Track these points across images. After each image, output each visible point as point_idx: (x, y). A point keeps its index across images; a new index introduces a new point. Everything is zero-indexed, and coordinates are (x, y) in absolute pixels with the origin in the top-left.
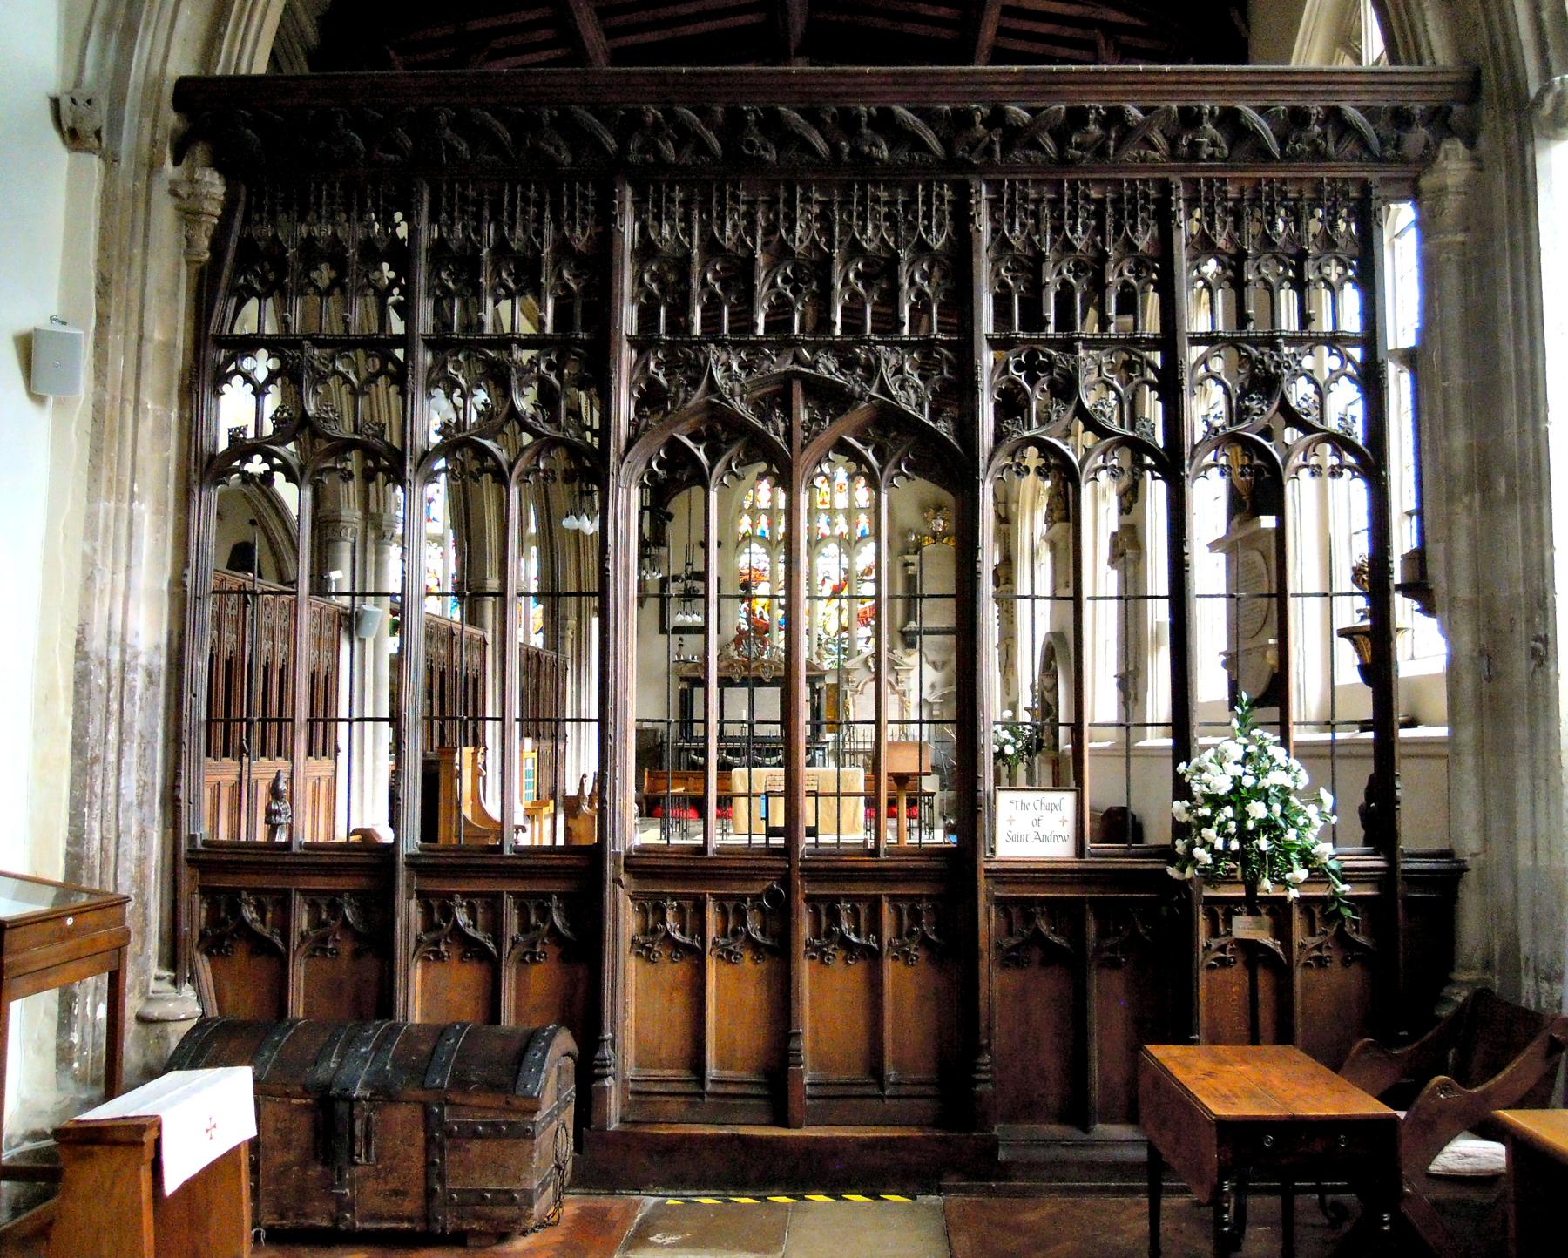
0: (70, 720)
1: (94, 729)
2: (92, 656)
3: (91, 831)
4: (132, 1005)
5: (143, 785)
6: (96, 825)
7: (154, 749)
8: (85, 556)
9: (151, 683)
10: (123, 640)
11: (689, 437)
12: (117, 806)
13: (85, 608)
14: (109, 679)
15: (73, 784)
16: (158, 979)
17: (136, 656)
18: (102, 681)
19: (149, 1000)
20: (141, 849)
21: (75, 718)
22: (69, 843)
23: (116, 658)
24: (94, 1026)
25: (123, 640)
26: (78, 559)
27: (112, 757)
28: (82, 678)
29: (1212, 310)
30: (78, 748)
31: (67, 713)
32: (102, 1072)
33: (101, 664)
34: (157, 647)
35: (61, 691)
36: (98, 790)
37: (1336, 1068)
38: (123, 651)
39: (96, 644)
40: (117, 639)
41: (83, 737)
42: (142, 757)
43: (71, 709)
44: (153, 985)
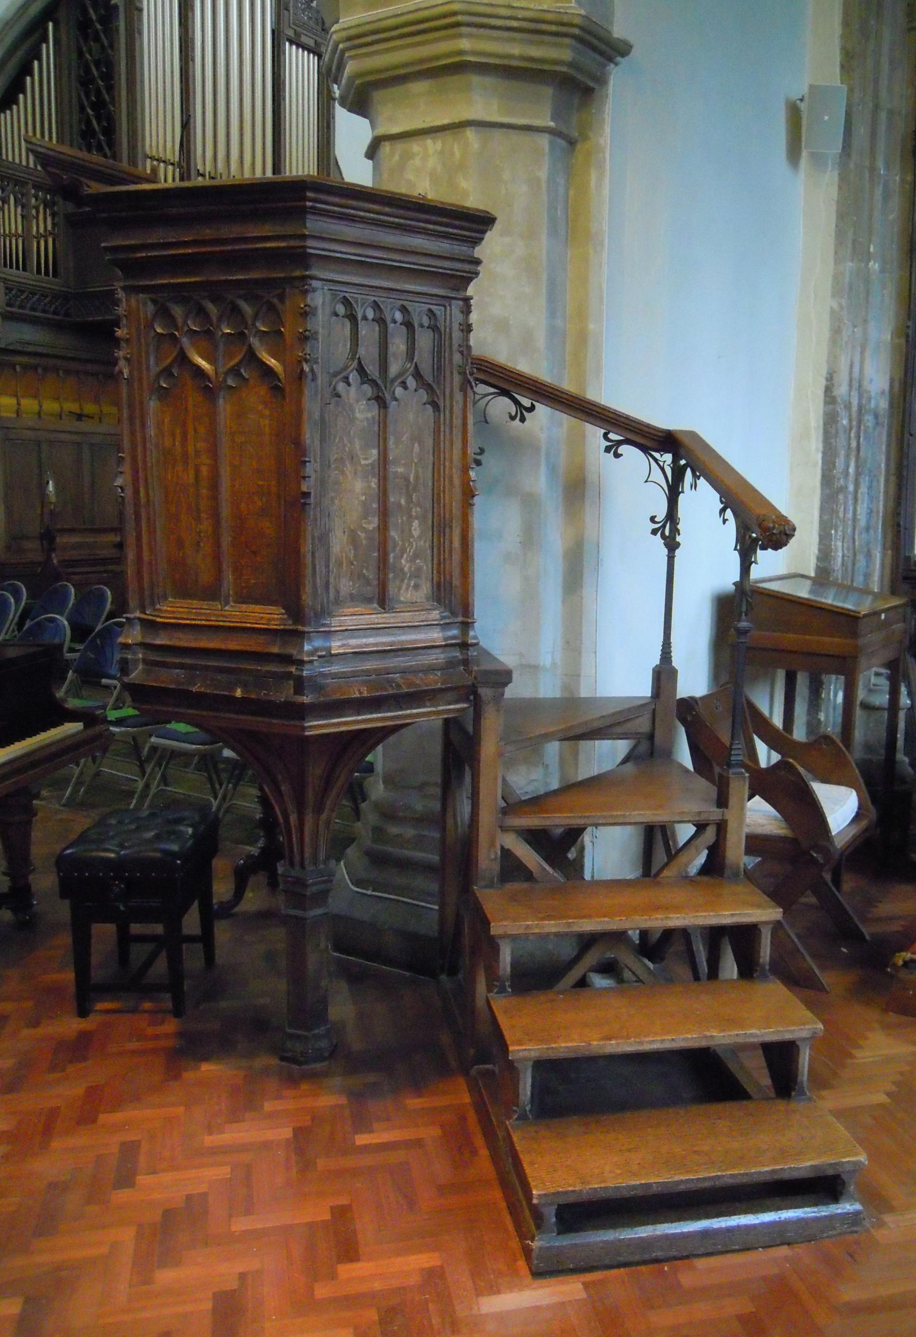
0: (820, 456)
1: (840, 462)
2: (839, 400)
3: (837, 550)
4: (861, 694)
5: (870, 512)
6: (839, 544)
7: (878, 481)
8: (832, 312)
9: (877, 424)
10: (860, 386)
11: (231, 359)
12: (854, 529)
13: (833, 359)
14: (850, 420)
15: (822, 509)
16: (877, 674)
17: (869, 399)
18: (845, 422)
19: (870, 691)
20: (867, 566)
21: (824, 454)
22: (818, 559)
23: (855, 402)
24: (834, 708)
25: (860, 386)
26: (826, 317)
27: (851, 488)
28: (830, 420)
29: (73, 359)
30: (827, 479)
31: (817, 450)
32: (406, 690)
33: (845, 406)
34: (883, 393)
35: (813, 431)
36: (841, 515)
37: (579, 676)
38: (860, 397)
39: (841, 390)
40: (855, 384)
41: (831, 471)
42: (870, 487)
43: (820, 446)
44: (873, 680)
